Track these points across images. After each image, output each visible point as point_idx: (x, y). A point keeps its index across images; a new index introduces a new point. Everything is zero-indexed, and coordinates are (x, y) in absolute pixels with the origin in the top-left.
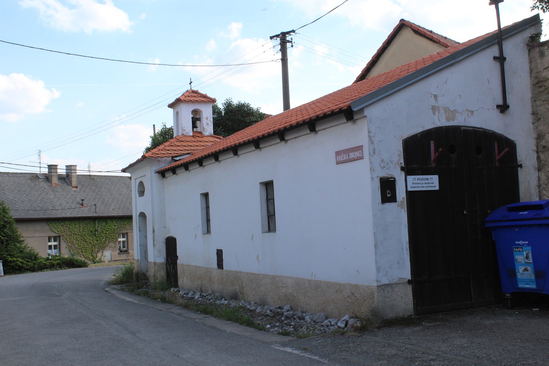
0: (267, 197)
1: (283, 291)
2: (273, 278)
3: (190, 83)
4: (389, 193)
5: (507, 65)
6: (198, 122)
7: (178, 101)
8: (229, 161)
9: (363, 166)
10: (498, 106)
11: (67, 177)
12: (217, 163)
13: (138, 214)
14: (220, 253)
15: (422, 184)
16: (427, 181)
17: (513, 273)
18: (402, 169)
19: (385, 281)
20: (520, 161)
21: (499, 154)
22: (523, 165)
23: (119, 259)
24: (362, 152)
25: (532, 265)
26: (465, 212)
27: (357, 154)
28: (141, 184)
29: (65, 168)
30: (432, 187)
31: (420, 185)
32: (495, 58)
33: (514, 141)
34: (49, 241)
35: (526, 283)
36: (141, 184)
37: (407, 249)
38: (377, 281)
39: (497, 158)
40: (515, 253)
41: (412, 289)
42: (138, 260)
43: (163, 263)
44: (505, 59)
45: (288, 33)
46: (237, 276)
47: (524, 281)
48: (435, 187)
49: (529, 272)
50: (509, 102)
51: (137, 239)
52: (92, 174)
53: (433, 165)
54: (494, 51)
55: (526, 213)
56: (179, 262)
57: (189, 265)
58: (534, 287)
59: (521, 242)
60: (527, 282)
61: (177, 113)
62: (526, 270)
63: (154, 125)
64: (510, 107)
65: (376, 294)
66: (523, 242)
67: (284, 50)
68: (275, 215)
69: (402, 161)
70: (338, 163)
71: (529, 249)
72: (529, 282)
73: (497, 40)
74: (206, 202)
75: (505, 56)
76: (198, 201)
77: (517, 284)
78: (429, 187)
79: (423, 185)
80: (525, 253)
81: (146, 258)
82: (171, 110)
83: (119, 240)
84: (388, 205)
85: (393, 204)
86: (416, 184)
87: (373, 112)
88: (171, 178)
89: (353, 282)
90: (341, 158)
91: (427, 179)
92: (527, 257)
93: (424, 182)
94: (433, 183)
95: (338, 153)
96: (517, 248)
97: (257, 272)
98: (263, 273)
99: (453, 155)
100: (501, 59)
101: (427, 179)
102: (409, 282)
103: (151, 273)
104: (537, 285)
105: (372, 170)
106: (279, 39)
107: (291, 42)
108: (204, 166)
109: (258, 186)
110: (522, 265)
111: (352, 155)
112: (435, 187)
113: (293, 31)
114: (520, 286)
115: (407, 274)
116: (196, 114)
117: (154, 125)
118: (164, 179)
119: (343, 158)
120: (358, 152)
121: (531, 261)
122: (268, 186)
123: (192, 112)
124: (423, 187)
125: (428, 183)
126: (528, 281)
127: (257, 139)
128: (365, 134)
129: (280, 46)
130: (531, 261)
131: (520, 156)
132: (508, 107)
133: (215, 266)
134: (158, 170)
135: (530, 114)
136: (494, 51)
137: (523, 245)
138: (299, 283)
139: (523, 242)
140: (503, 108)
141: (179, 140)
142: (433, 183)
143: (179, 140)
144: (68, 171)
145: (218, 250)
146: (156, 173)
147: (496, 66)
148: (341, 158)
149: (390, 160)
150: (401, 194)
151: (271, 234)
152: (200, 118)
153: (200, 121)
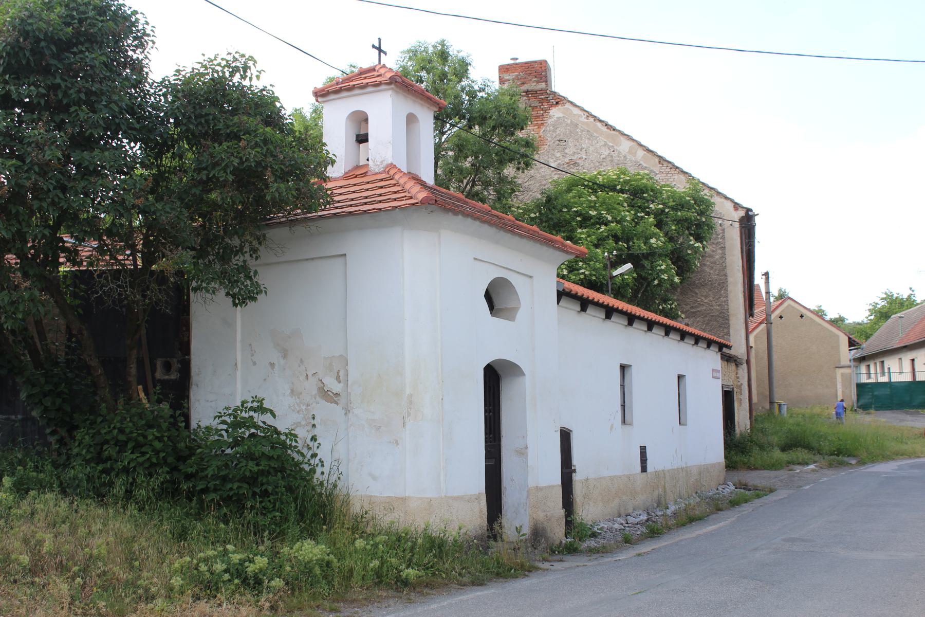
14: (643, 450)
95: (713, 370)
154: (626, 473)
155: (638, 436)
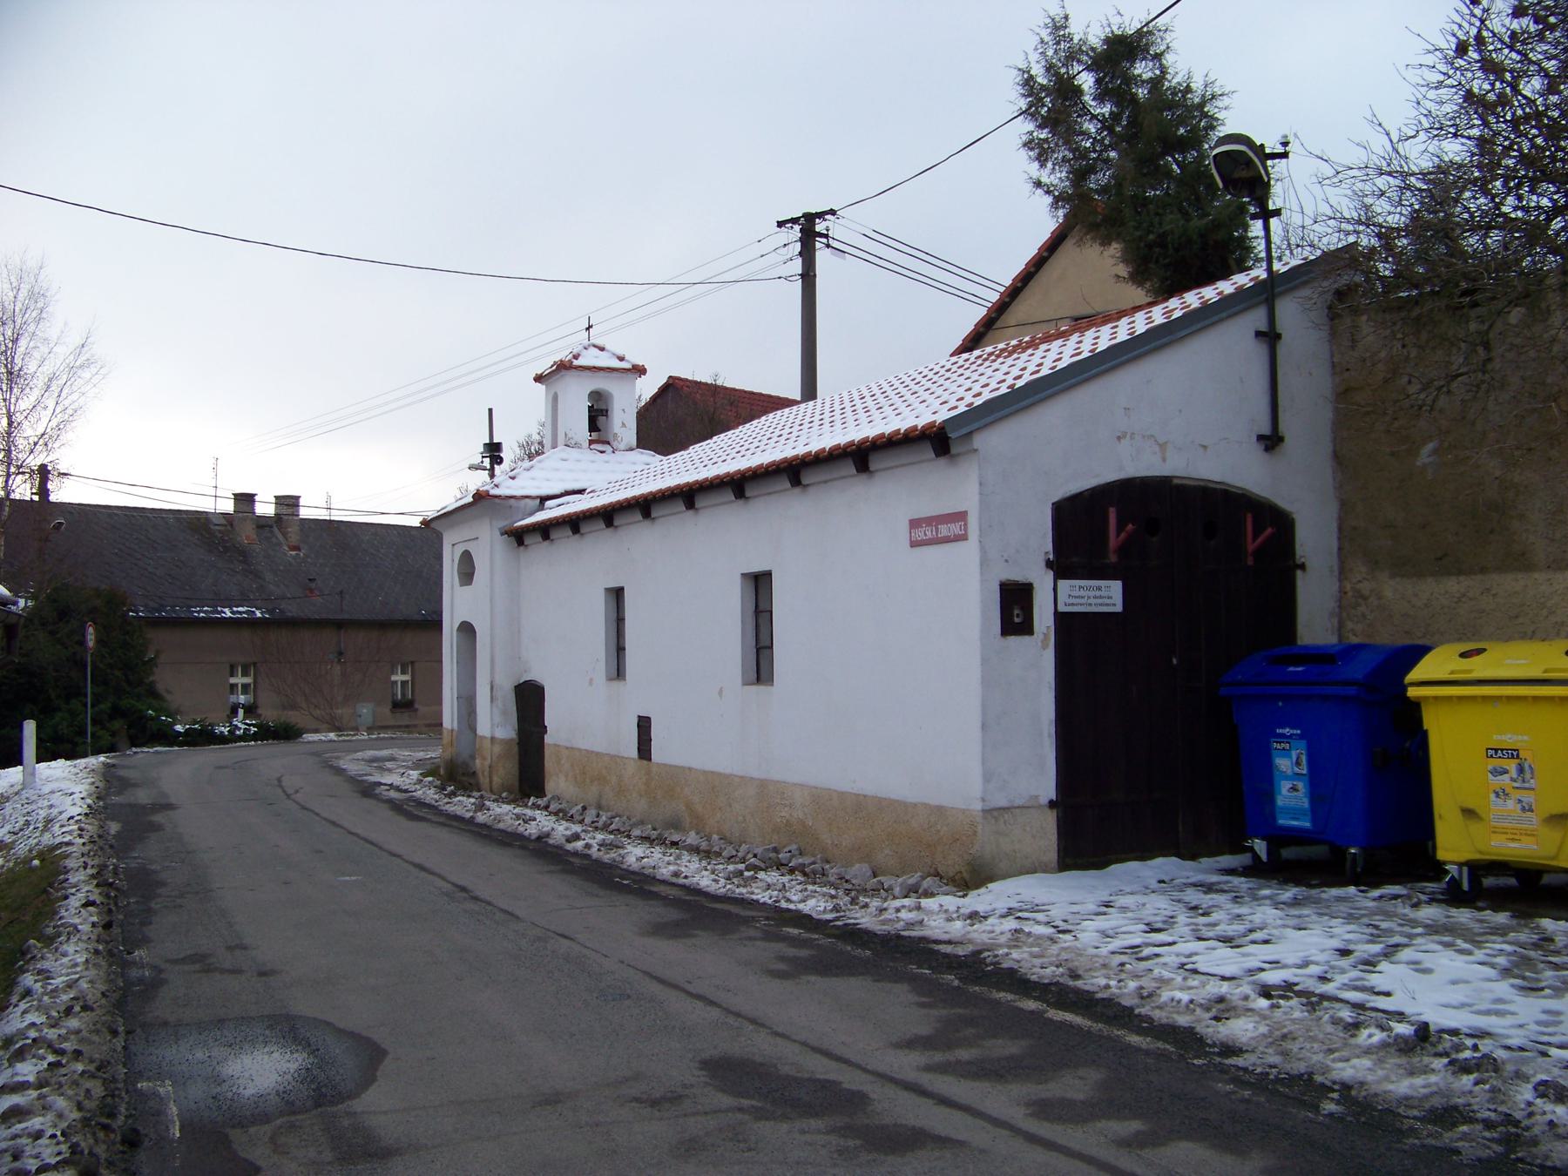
0: (757, 606)
1: (783, 814)
2: (763, 784)
3: (588, 329)
4: (1018, 616)
5: (1282, 349)
6: (601, 419)
7: (563, 367)
8: (676, 527)
9: (968, 552)
10: (1260, 438)
11: (276, 522)
12: (647, 523)
13: (456, 626)
14: (644, 725)
15: (1089, 597)
16: (1098, 593)
17: (1269, 794)
18: (1049, 564)
19: (1002, 802)
20: (1301, 557)
21: (1255, 537)
22: (1307, 564)
23: (392, 723)
24: (966, 525)
25: (1306, 778)
26: (1175, 661)
27: (955, 529)
29: (273, 500)
30: (1107, 605)
31: (1082, 601)
32: (1258, 334)
33: (1291, 513)
34: (232, 676)
35: (1511, 836)
37: (1049, 736)
38: (983, 800)
39: (1251, 547)
40: (1274, 752)
41: (1058, 820)
42: (452, 730)
43: (512, 740)
44: (1278, 336)
45: (821, 215)
46: (677, 775)
47: (1506, 833)
48: (1114, 605)
49: (1300, 794)
50: (1283, 428)
52: (332, 518)
53: (1113, 558)
54: (1256, 319)
55: (1300, 669)
56: (548, 739)
57: (572, 748)
58: (1307, 824)
59: (1287, 731)
60: (1295, 813)
61: (555, 399)
62: (1294, 789)
63: (490, 411)
64: (1286, 439)
65: (980, 827)
66: (1292, 732)
67: (808, 254)
68: (771, 647)
69: (1049, 547)
70: (914, 544)
71: (1303, 744)
72: (1521, 834)
73: (1264, 296)
74: (618, 608)
75: (1279, 329)
77: (1274, 818)
78: (1101, 605)
79: (1089, 601)
80: (1294, 754)
81: (473, 728)
82: (541, 387)
83: (394, 678)
84: (1013, 640)
85: (1026, 639)
86: (1076, 597)
87: (992, 441)
88: (538, 550)
89: (933, 802)
90: (919, 535)
91: (1099, 588)
92: (1298, 763)
93: (1092, 593)
94: (1111, 598)
95: (915, 524)
96: (1280, 743)
97: (728, 771)
98: (740, 774)
99: (1155, 539)
100: (1270, 337)
101: (1099, 588)
102: (1052, 804)
104: (1314, 820)
105: (984, 562)
106: (797, 228)
107: (826, 236)
108: (616, 527)
109: (738, 579)
110: (1287, 778)
111: (944, 530)
112: (1114, 605)
113: (832, 212)
114: (1281, 822)
115: (1045, 786)
116: (597, 401)
117: (490, 411)
118: (522, 548)
119: (925, 535)
120: (958, 525)
121: (1305, 772)
122: (760, 583)
123: (591, 392)
124: (1090, 605)
125: (1101, 597)
126: (1518, 832)
127: (738, 479)
128: (972, 489)
129: (799, 244)
130: (1305, 772)
131: (1302, 545)
132: (1281, 439)
133: (634, 753)
134: (506, 529)
136: (1256, 319)
137: (1291, 736)
138: (821, 799)
139: (1292, 732)
140: (1271, 441)
142: (1111, 598)
144: (285, 511)
145: (640, 717)
146: (502, 534)
147: (1259, 351)
148: (919, 535)
150: (1043, 618)
151: (761, 688)
152: (607, 411)
153: (607, 416)
154: (613, 752)
155: (636, 697)
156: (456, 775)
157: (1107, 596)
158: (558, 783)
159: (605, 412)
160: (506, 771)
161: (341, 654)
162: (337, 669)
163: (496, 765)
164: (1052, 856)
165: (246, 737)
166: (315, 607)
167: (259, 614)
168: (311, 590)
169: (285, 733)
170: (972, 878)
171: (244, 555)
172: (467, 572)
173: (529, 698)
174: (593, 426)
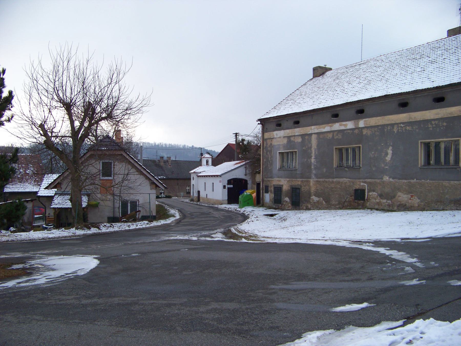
23: (186, 196)
28: (193, 177)
36: (193, 177)
51: (431, 154)
76: (204, 184)
84: (224, 189)
88: (199, 177)
100: (246, 167)
103: (194, 199)
115: (227, 199)
135: (312, 118)
140: (246, 175)
141: (58, 93)
143: (58, 93)
149: (343, 228)
150: (227, 188)
155: (206, 192)
156: (192, 200)
157: (232, 186)
158: (201, 200)
159: (208, 162)
160: (197, 199)
161: (178, 184)
162: (177, 187)
163: (195, 199)
164: (227, 203)
165: (164, 197)
166: (174, 176)
167: (165, 178)
168: (173, 173)
169: (169, 197)
170: (222, 204)
171: (161, 167)
172: (193, 179)
173: (199, 192)
174: (207, 163)
